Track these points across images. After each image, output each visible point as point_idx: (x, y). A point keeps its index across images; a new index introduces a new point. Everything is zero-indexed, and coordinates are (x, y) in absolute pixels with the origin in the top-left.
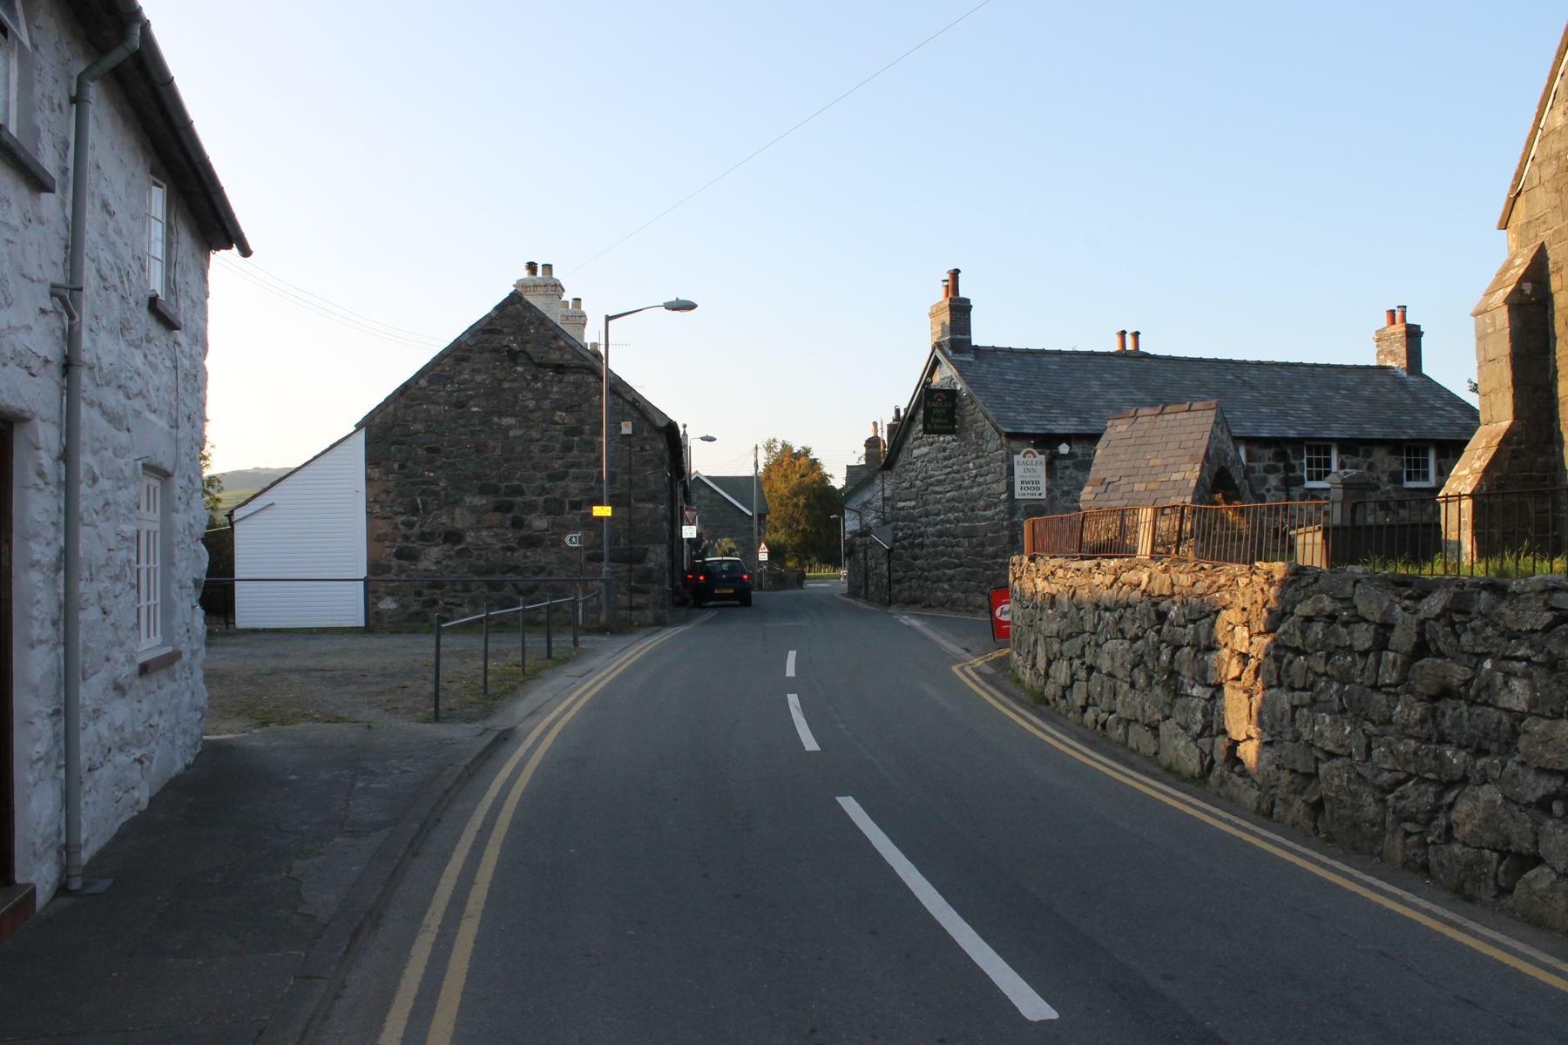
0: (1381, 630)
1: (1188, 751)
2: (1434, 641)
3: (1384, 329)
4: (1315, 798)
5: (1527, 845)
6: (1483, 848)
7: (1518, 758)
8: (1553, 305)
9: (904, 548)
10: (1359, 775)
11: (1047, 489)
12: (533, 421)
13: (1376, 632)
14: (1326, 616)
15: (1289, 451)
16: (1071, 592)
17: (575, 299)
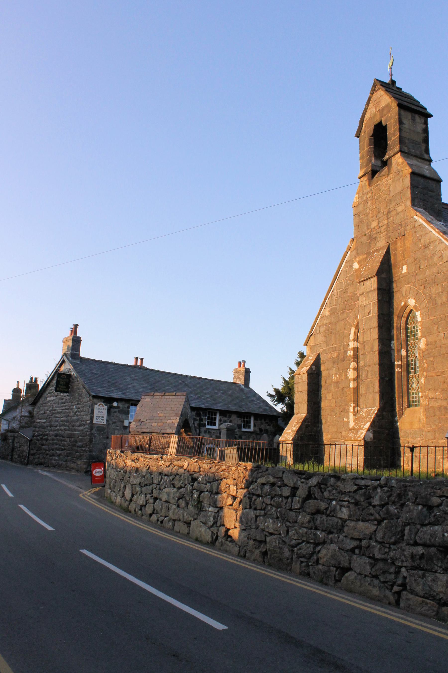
0: (293, 489)
1: (206, 532)
2: (314, 494)
3: (237, 369)
4: (264, 550)
5: (346, 564)
6: (330, 566)
7: (344, 534)
8: (321, 375)
9: (38, 440)
10: (283, 541)
11: (107, 420)
13: (291, 490)
14: (271, 484)
15: (201, 413)
16: (148, 467)
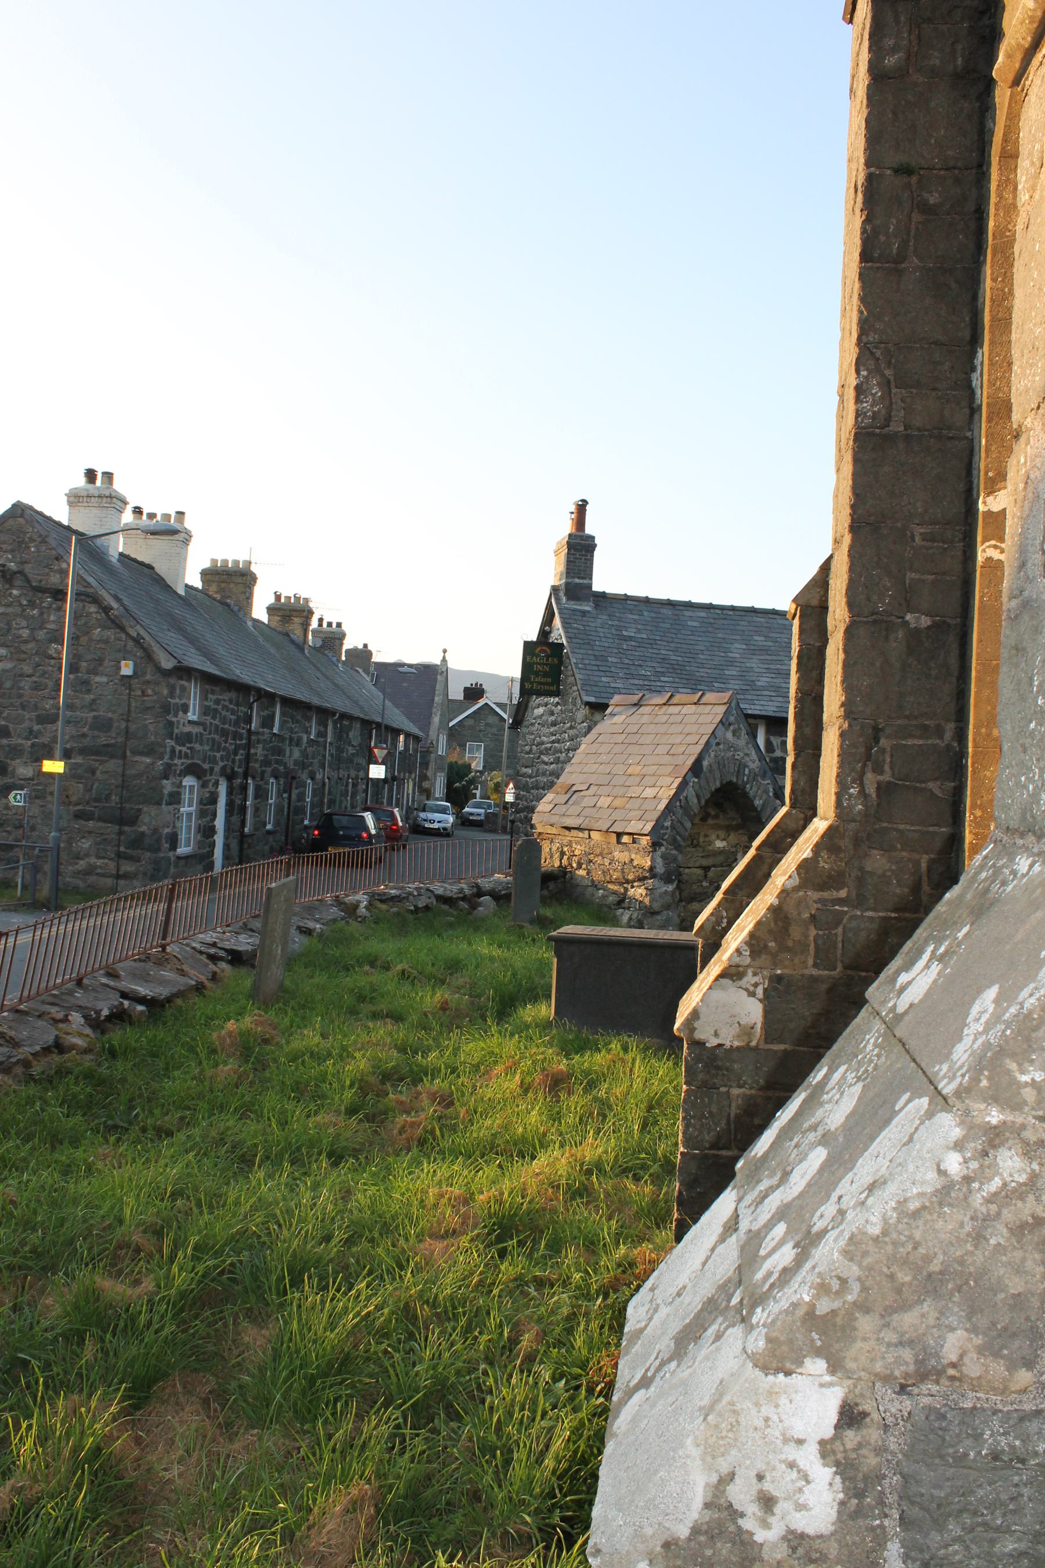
12: (25, 653)
17: (178, 513)
